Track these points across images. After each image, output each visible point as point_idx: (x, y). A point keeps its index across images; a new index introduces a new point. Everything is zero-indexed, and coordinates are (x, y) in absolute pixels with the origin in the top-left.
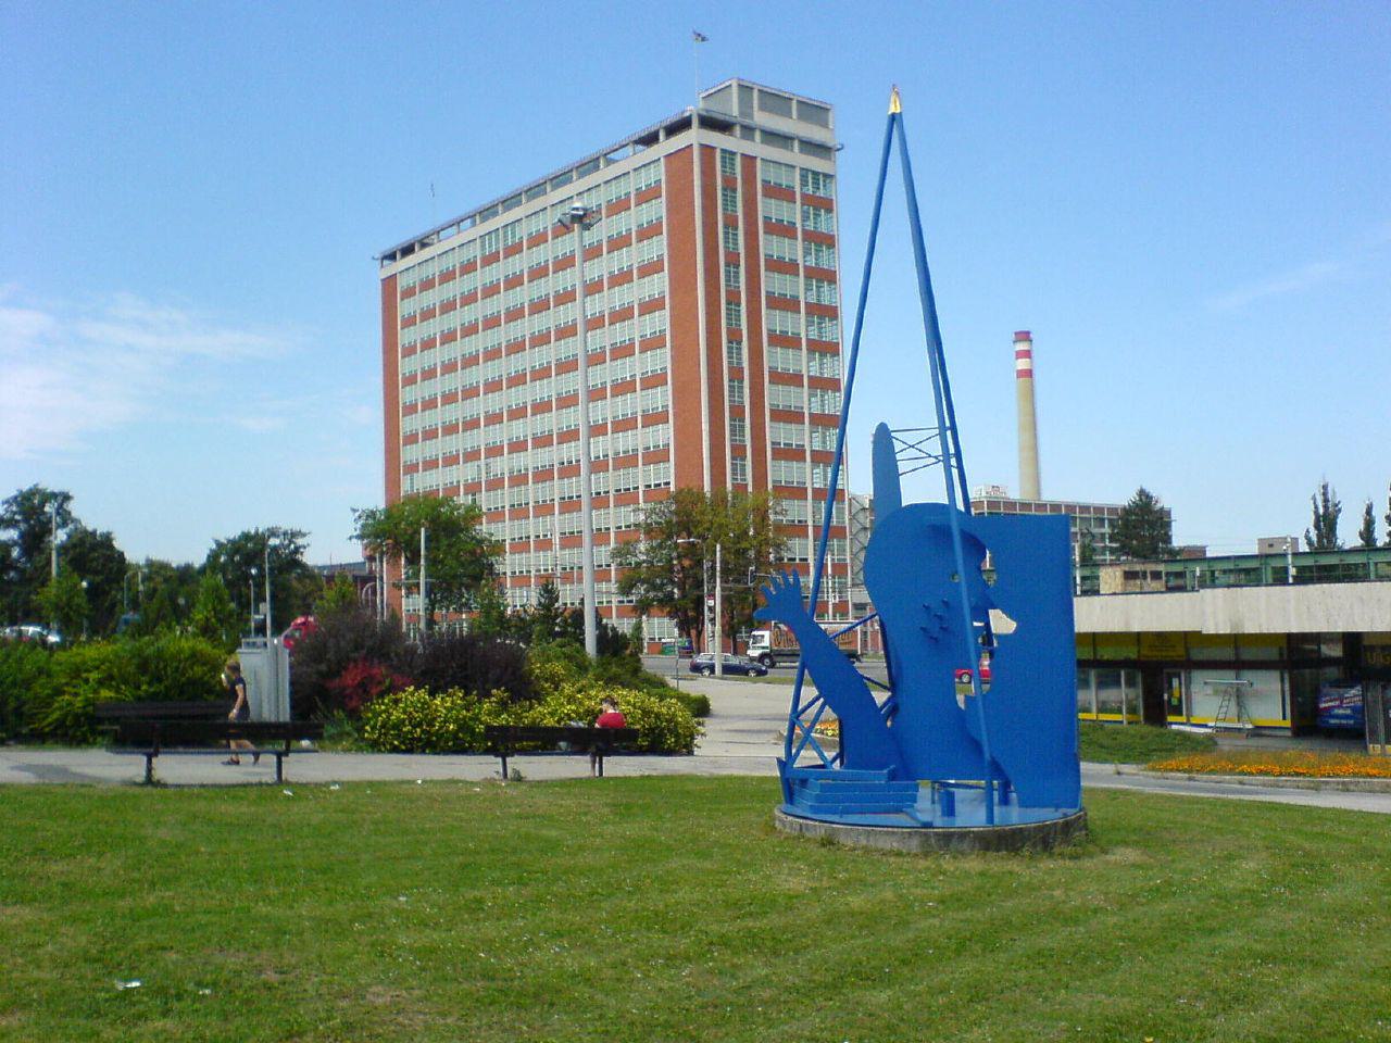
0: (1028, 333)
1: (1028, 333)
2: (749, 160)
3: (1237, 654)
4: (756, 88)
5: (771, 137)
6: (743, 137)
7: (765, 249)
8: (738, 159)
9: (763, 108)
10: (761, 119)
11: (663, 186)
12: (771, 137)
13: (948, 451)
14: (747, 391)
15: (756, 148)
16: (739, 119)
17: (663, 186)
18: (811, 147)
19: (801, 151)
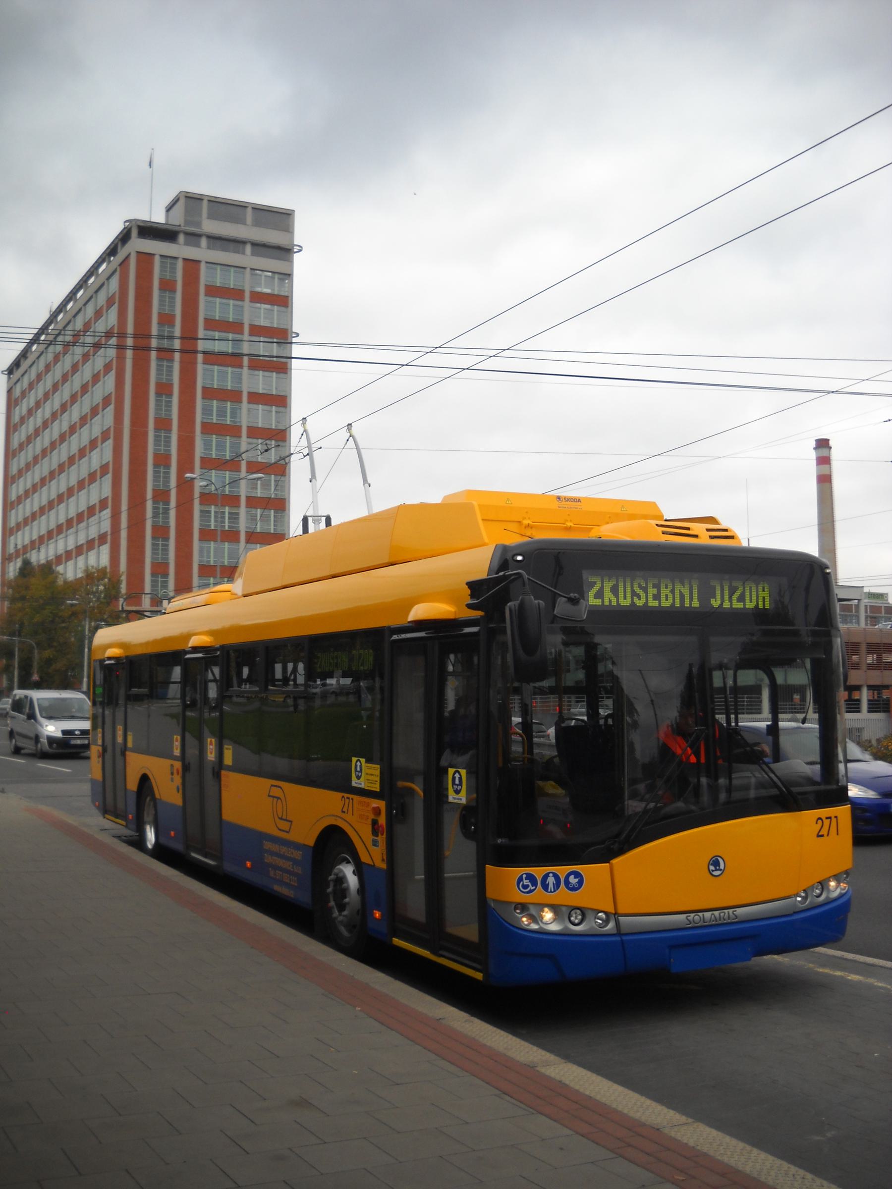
0: (827, 441)
1: (827, 441)
2: (192, 265)
3: (786, 680)
4: (206, 199)
5: (217, 241)
6: (187, 243)
7: (204, 379)
8: (180, 264)
9: (211, 216)
10: (210, 226)
11: (791, 628)
12: (217, 241)
13: (226, 354)
14: (172, 514)
15: (202, 253)
16: (183, 228)
17: (791, 628)
18: (261, 248)
19: (253, 254)
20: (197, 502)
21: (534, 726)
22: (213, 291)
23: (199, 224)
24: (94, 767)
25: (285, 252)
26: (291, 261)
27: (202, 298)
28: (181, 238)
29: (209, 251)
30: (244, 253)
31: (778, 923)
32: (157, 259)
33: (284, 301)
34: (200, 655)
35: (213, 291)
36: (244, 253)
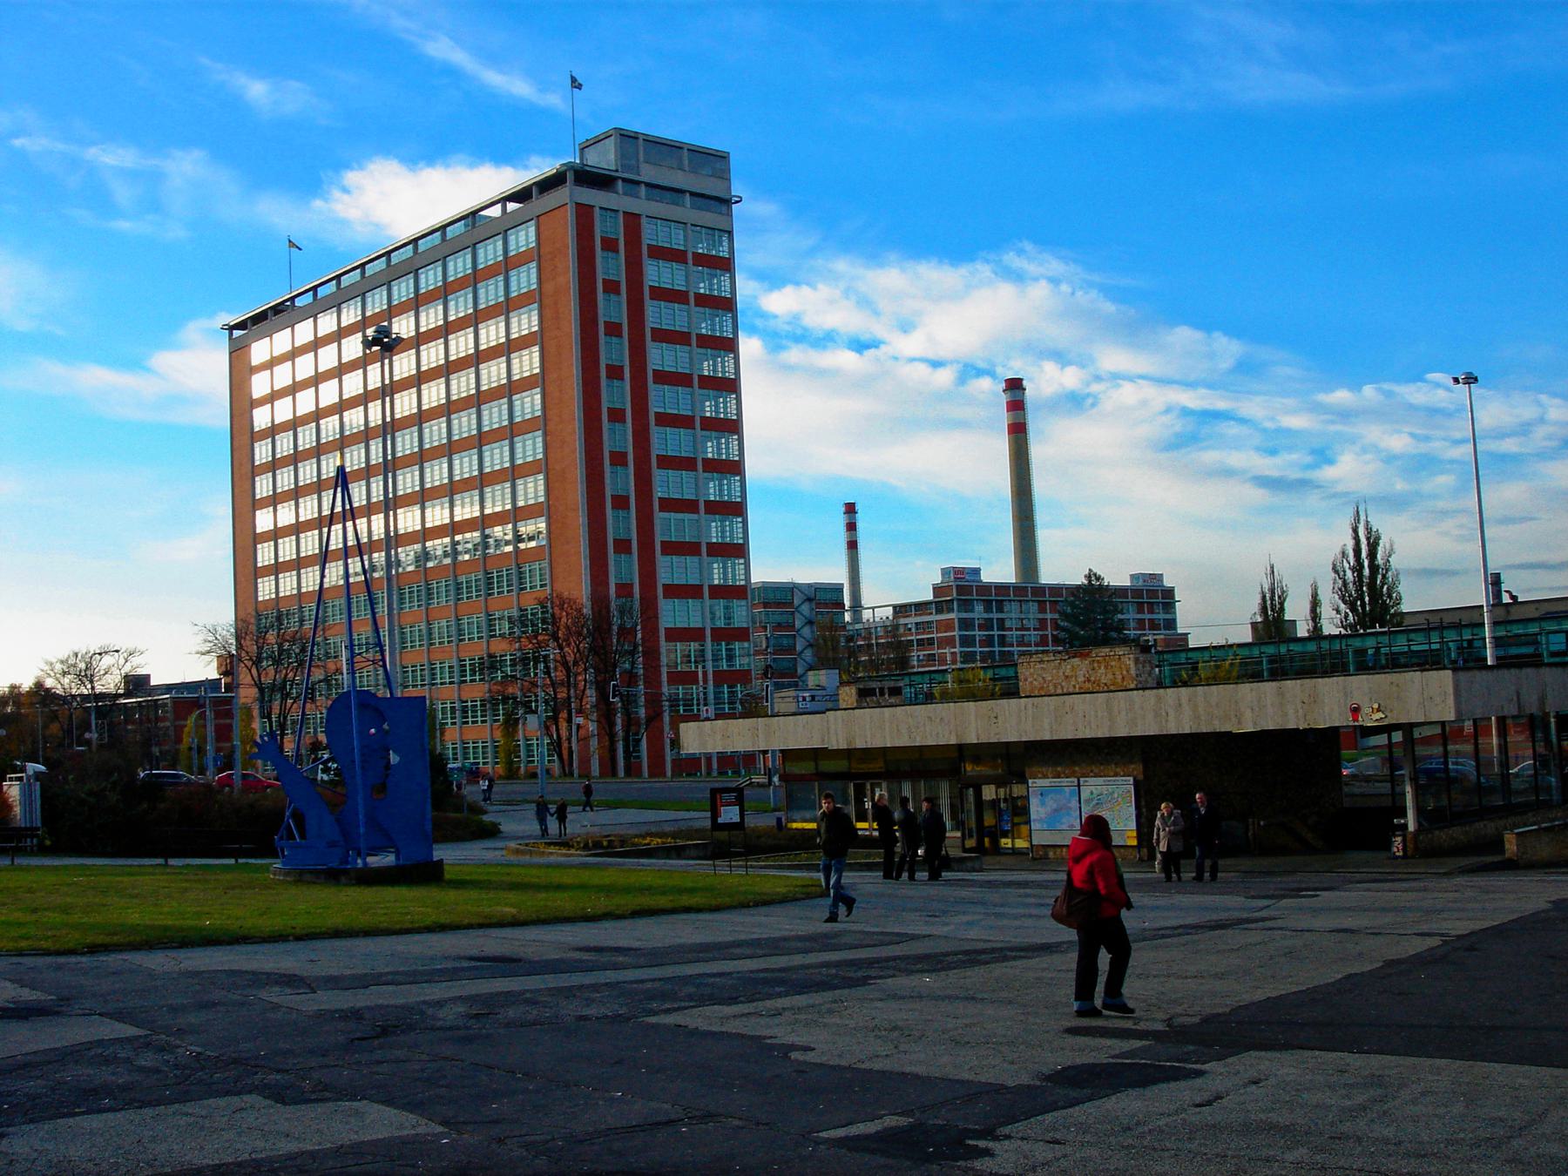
10: (648, 173)
25: (725, 202)
26: (730, 214)
32: (597, 210)
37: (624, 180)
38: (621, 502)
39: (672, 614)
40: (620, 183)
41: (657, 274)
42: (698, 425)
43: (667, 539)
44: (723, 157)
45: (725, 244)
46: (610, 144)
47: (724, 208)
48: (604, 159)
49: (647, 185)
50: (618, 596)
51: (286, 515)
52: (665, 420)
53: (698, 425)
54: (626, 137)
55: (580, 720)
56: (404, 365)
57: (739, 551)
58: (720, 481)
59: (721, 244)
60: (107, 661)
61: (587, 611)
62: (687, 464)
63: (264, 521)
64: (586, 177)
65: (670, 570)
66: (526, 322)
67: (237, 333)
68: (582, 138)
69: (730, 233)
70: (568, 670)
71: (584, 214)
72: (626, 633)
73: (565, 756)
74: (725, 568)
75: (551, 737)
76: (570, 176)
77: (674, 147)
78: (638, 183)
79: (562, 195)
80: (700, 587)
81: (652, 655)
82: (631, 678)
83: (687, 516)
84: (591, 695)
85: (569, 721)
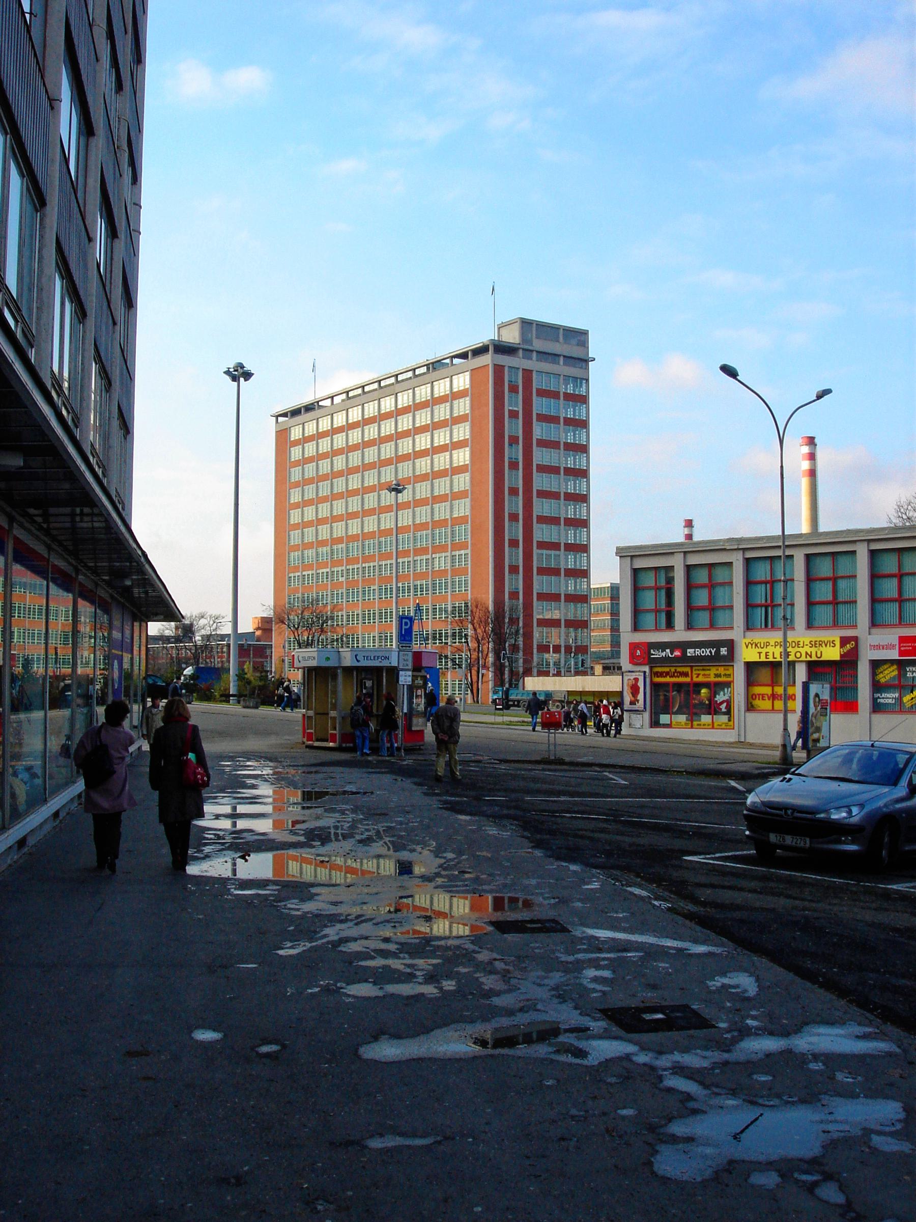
2: (528, 374)
5: (543, 355)
10: (538, 345)
12: (543, 355)
15: (532, 364)
16: (522, 346)
20: (535, 651)
21: (410, 667)
22: (542, 393)
23: (530, 342)
24: (231, 876)
25: (584, 361)
26: (587, 368)
27: (536, 551)
28: (521, 352)
29: (539, 363)
30: (559, 364)
31: (127, 540)
32: (506, 369)
33: (583, 400)
34: (660, 1016)
35: (542, 393)
36: (559, 364)
37: (523, 349)
38: (514, 440)
39: (542, 611)
40: (521, 351)
41: (540, 405)
42: (562, 472)
43: (539, 412)
44: (585, 333)
45: (584, 385)
46: (516, 328)
47: (584, 364)
48: (512, 336)
49: (537, 352)
50: (510, 598)
51: (310, 513)
52: (543, 494)
53: (562, 472)
54: (526, 324)
55: (484, 671)
56: (388, 475)
57: (584, 574)
58: (575, 506)
59: (581, 386)
60: (203, 622)
61: (491, 608)
62: (554, 521)
63: (295, 517)
64: (501, 348)
65: (540, 584)
66: (462, 432)
67: (281, 419)
68: (498, 322)
69: (587, 380)
70: (479, 642)
71: (499, 370)
72: (513, 621)
73: (475, 691)
74: (575, 558)
75: (467, 679)
76: (491, 349)
77: (554, 328)
78: (532, 351)
79: (487, 359)
80: (559, 468)
81: (528, 636)
82: (515, 648)
83: (553, 552)
84: (491, 659)
85: (478, 672)
